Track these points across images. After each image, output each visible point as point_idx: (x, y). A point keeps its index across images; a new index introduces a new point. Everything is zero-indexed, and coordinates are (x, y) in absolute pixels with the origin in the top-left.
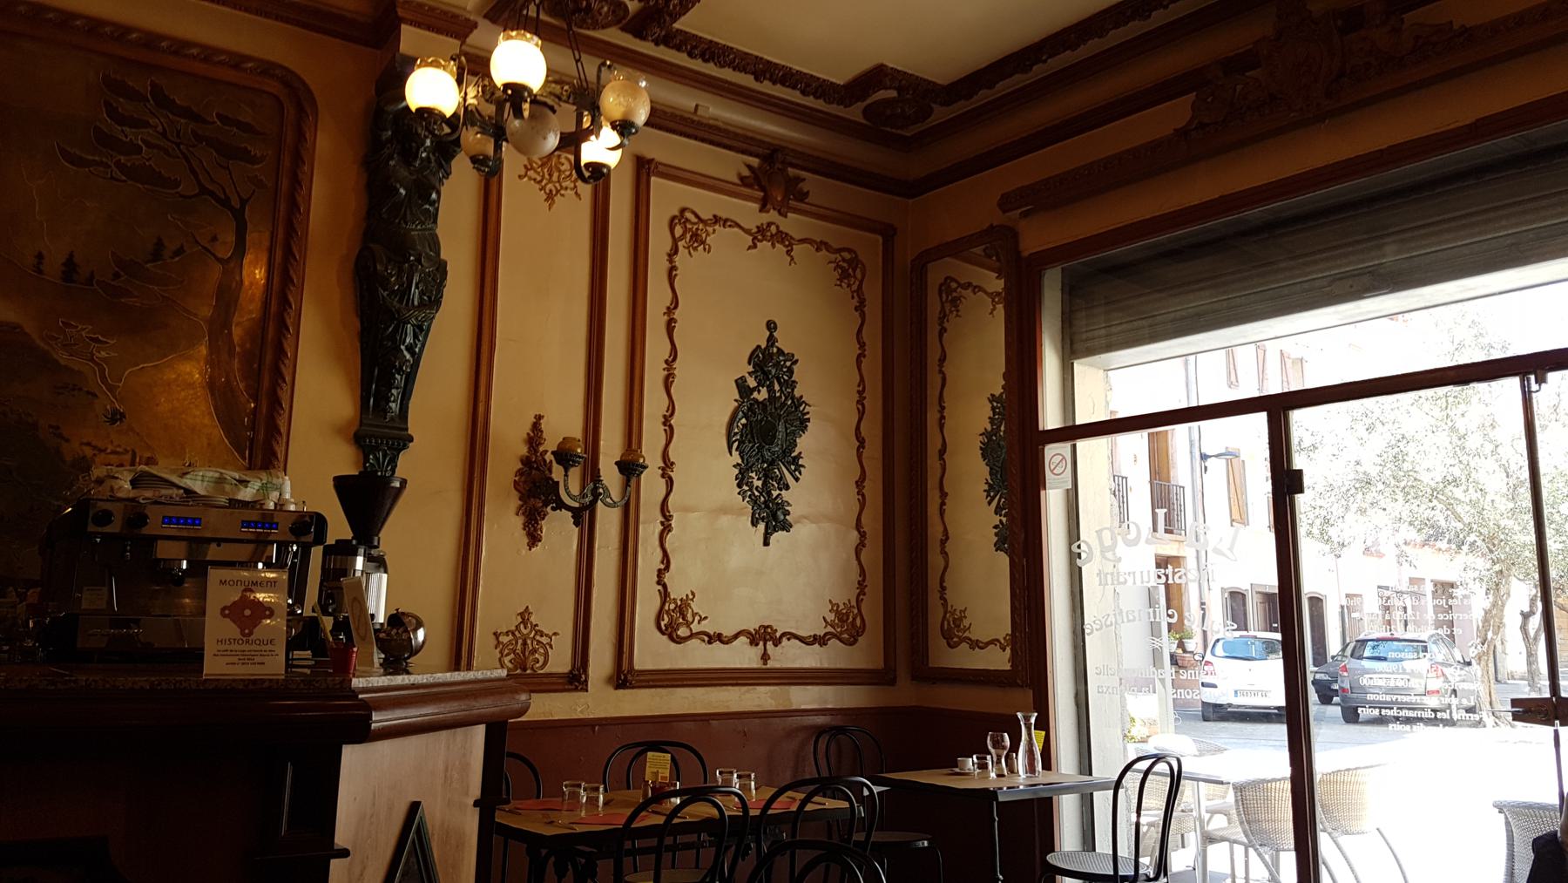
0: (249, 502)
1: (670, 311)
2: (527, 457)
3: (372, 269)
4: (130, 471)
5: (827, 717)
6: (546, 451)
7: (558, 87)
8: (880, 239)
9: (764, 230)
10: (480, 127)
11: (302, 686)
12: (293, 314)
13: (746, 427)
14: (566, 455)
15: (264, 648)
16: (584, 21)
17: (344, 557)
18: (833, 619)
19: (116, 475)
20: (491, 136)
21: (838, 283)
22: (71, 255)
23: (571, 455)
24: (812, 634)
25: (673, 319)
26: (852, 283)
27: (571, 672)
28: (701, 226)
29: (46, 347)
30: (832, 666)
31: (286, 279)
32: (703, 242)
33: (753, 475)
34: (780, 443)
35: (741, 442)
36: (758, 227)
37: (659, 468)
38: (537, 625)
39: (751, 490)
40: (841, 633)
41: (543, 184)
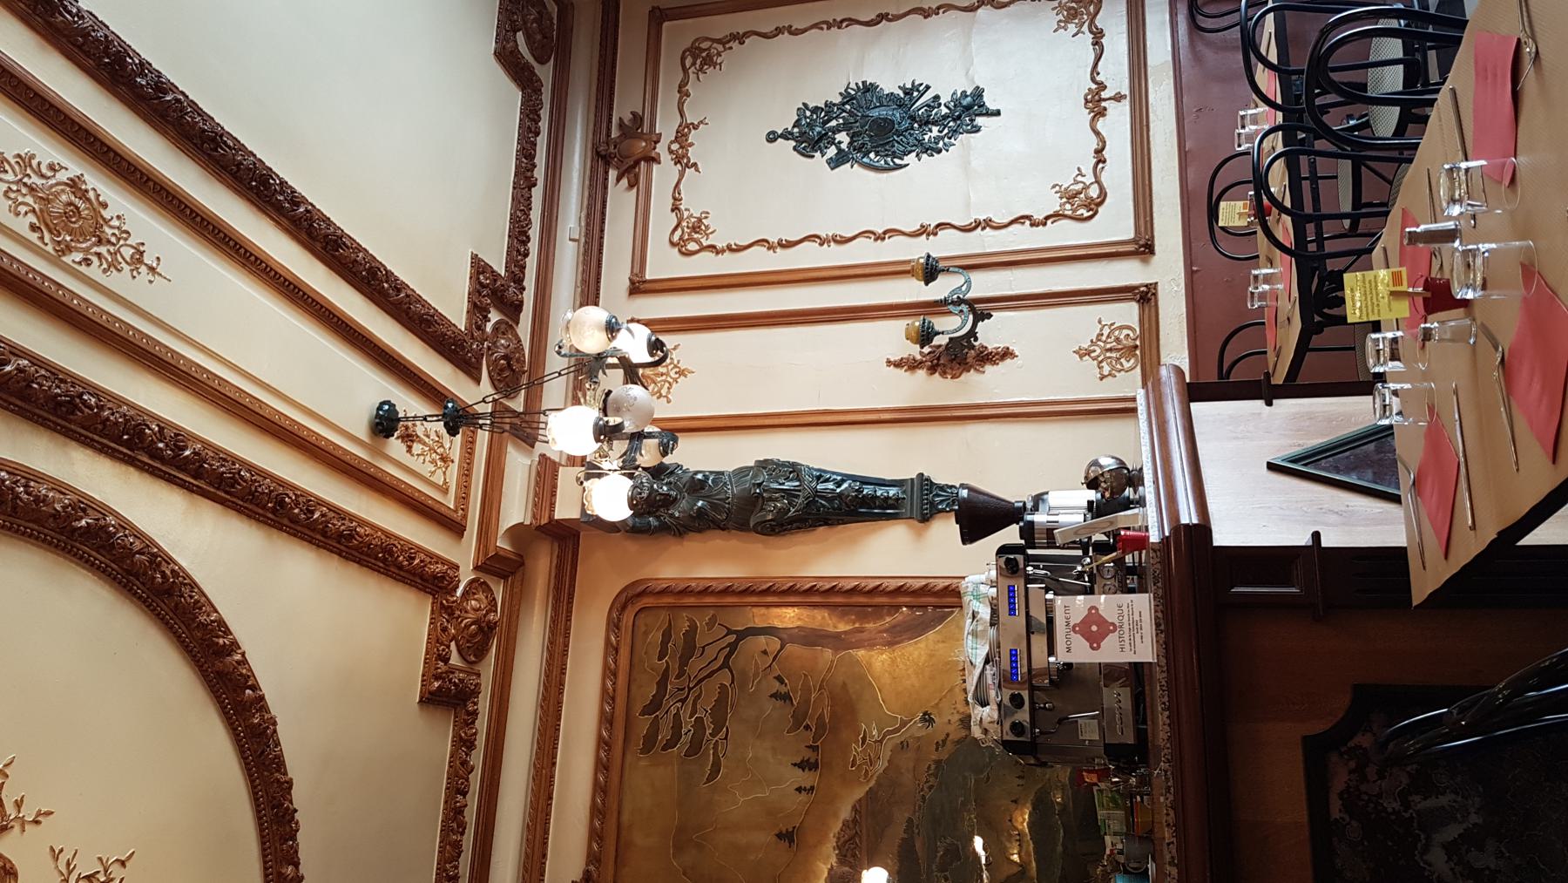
0: (992, 609)
1: (771, 247)
2: (928, 369)
3: (773, 523)
4: (973, 708)
5: (1178, 6)
7: (588, 393)
8: (666, 24)
9: (676, 157)
10: (635, 452)
11: (1159, 585)
12: (821, 584)
13: (878, 152)
14: (923, 336)
15: (1126, 613)
16: (518, 361)
17: (1036, 531)
18: (1074, 25)
19: (979, 719)
20: (641, 443)
21: (718, 67)
23: (923, 331)
24: (1091, 47)
25: (778, 243)
26: (716, 52)
27: (1138, 301)
28: (684, 224)
29: (875, 778)
30: (1125, 19)
31: (791, 591)
32: (700, 220)
33: (926, 137)
34: (891, 113)
35: (894, 155)
36: (676, 164)
37: (928, 239)
38: (1092, 341)
39: (943, 138)
40: (1088, 14)
41: (671, 380)
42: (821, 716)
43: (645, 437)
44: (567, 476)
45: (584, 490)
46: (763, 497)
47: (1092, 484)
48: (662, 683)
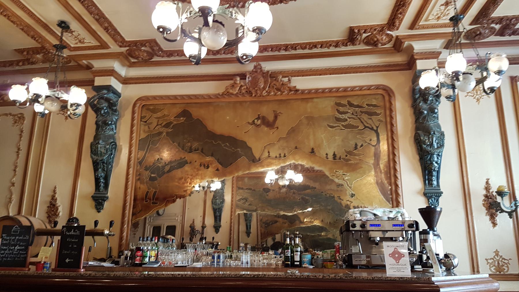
3: (419, 139)
6: (493, 192)
11: (416, 279)
15: (403, 267)
16: (479, 38)
22: (334, 152)
31: (394, 147)
38: (502, 256)
42: (350, 160)
43: (453, 90)
44: (433, 63)
45: (431, 70)
46: (429, 135)
47: (446, 256)
48: (358, 106)
